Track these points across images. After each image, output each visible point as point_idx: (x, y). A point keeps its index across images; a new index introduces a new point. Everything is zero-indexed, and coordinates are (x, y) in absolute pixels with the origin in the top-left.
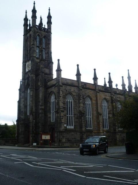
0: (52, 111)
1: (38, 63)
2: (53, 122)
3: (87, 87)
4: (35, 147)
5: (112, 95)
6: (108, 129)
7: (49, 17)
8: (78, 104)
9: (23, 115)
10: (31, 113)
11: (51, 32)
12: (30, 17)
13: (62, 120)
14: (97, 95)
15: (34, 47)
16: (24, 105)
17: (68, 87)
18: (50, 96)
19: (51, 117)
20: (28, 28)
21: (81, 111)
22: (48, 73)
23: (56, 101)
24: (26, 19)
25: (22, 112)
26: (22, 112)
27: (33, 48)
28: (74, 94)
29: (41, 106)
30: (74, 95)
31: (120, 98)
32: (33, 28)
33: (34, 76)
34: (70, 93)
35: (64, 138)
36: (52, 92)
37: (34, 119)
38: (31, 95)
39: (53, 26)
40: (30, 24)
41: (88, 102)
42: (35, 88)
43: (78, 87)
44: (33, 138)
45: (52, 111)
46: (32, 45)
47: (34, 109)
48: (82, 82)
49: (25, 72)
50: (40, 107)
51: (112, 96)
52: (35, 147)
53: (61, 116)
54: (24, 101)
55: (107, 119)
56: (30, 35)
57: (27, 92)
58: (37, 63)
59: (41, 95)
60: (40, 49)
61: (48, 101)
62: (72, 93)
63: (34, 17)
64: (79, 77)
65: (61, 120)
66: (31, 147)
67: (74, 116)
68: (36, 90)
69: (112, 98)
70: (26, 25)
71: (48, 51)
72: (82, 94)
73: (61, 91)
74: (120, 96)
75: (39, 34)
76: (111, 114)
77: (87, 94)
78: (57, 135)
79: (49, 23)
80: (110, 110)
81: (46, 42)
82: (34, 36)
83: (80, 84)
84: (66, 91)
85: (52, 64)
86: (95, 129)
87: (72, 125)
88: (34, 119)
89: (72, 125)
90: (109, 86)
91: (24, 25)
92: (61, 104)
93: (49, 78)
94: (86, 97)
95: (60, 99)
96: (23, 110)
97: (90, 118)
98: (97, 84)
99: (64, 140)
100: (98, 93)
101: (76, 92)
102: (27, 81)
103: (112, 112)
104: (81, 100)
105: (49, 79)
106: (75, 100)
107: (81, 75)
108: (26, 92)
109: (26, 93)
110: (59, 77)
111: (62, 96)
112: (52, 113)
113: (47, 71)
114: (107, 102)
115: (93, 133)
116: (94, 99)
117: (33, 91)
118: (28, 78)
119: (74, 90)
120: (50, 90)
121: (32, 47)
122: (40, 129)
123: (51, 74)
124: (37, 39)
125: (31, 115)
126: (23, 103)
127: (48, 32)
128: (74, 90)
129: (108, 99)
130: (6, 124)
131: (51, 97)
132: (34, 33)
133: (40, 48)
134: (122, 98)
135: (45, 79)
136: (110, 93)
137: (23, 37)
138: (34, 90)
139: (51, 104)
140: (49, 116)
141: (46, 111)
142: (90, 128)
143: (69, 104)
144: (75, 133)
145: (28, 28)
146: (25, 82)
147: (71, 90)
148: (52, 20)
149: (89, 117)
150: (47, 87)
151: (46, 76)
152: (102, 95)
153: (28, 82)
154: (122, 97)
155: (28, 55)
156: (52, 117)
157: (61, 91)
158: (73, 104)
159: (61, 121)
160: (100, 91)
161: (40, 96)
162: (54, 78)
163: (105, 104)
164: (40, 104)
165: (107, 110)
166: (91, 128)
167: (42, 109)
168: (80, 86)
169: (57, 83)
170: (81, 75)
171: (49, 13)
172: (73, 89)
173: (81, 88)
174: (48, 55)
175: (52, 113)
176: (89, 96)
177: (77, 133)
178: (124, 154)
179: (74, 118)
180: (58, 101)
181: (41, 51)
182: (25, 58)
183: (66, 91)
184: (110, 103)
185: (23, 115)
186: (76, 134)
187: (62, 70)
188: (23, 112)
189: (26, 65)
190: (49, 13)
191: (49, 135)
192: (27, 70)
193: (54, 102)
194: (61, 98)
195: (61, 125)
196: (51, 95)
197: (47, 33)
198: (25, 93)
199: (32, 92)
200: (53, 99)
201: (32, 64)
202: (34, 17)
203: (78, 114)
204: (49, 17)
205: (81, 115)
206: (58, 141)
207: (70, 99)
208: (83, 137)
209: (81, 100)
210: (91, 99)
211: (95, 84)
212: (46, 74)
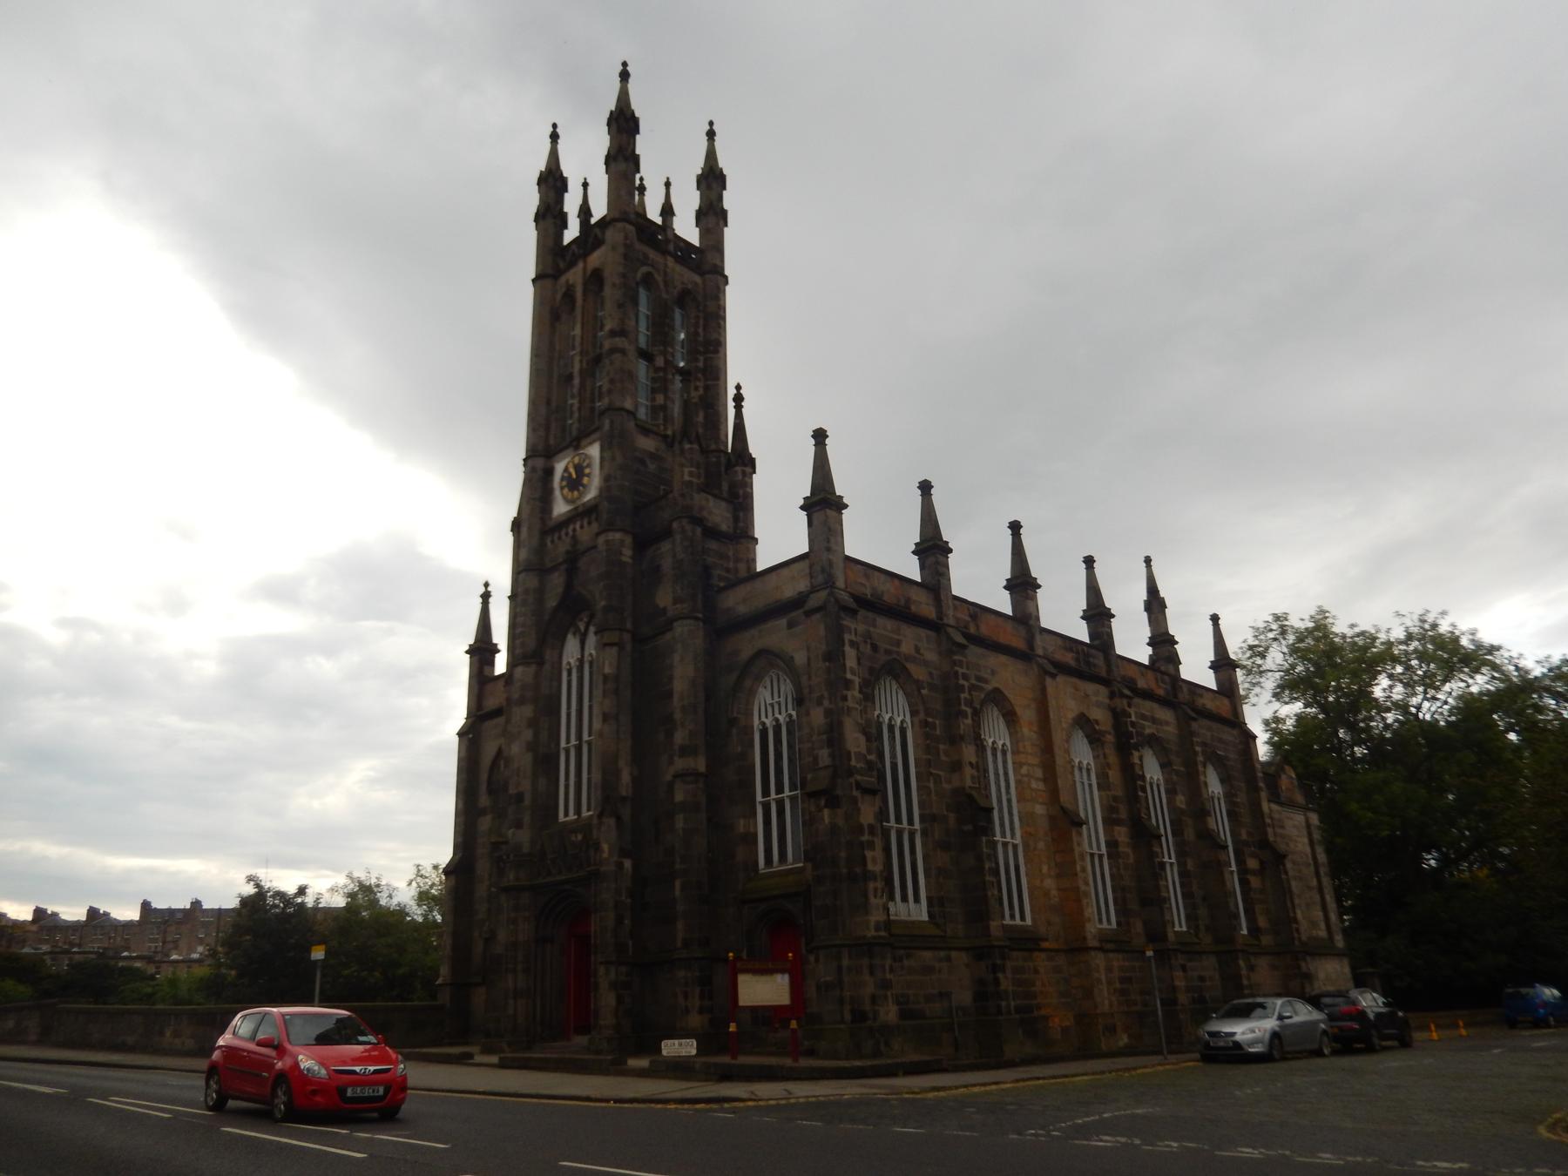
0: (766, 793)
1: (648, 461)
2: (779, 874)
3: (984, 630)
4: (680, 1069)
5: (1122, 696)
6: (1114, 925)
7: (712, 179)
8: (942, 747)
9: (527, 819)
10: (608, 801)
11: (723, 268)
12: (586, 165)
13: (869, 854)
14: (1043, 690)
15: (623, 352)
16: (532, 747)
17: (885, 626)
18: (748, 683)
19: (756, 835)
20: (572, 232)
21: (970, 797)
22: (724, 527)
23: (818, 717)
24: (552, 181)
25: (519, 797)
26: (519, 797)
27: (617, 356)
28: (918, 672)
29: (685, 751)
30: (919, 684)
31: (1154, 720)
32: (620, 225)
33: (628, 540)
34: (895, 669)
35: (886, 997)
36: (769, 658)
37: (624, 853)
38: (607, 670)
39: (732, 237)
40: (585, 211)
41: (996, 733)
42: (629, 626)
43: (936, 626)
44: (620, 1000)
45: (766, 793)
46: (613, 333)
47: (626, 777)
48: (956, 598)
49: (543, 520)
50: (680, 764)
51: (1121, 703)
52: (680, 1069)
53: (861, 827)
54: (533, 723)
55: (1101, 856)
56: (596, 279)
57: (560, 657)
58: (642, 462)
59: (683, 673)
60: (657, 370)
61: (733, 722)
62: (908, 665)
63: (622, 158)
64: (937, 563)
65: (864, 858)
66: (641, 1074)
67: (924, 833)
68: (642, 645)
69: (1118, 716)
70: (550, 215)
71: (706, 388)
72: (965, 677)
73: (847, 648)
74: (1155, 706)
75: (649, 274)
76: (1118, 822)
77: (986, 681)
78: (840, 969)
79: (712, 214)
80: (1115, 799)
81: (696, 334)
82: (624, 276)
83: (951, 612)
84: (875, 648)
85: (748, 470)
86: (1049, 923)
87: (917, 900)
88: (624, 853)
89: (917, 900)
90: (1091, 636)
91: (539, 217)
92: (854, 741)
93: (731, 565)
94: (983, 703)
95: (845, 698)
96: (526, 786)
97: (1015, 846)
98: (1038, 619)
99: (889, 1013)
100: (1049, 680)
101: (926, 663)
102: (557, 581)
103: (1123, 815)
104: (965, 715)
105: (728, 570)
106: (928, 714)
107: (951, 551)
108: (549, 655)
109: (547, 667)
110: (829, 549)
111: (857, 680)
112: (767, 807)
113: (718, 513)
114: (1095, 739)
115: (1043, 955)
116: (1027, 715)
117: (620, 645)
118: (572, 562)
119: (917, 650)
120: (746, 644)
121: (613, 350)
122: (680, 925)
123: (742, 535)
124: (626, 320)
125: (612, 822)
126: (528, 735)
127: (703, 269)
128: (917, 650)
129: (1097, 722)
130: (364, 894)
131: (752, 693)
132: (625, 256)
133: (660, 362)
134: (1167, 723)
135: (707, 570)
136: (1105, 682)
137: (528, 293)
138: (627, 637)
139: (752, 740)
140: (741, 825)
141: (725, 787)
142: (1018, 921)
143: (892, 738)
144: (942, 954)
145: (572, 232)
146: (540, 592)
147: (898, 643)
148: (729, 200)
149: (1011, 830)
150: (720, 628)
151: (713, 545)
152: (1067, 699)
153: (569, 586)
154: (1165, 714)
155: (560, 415)
156: (775, 840)
157: (853, 644)
158: (916, 746)
159: (865, 863)
160: (1063, 669)
161: (679, 686)
162: (760, 568)
163: (1082, 753)
164: (680, 737)
165: (1015, 812)
166: (1023, 918)
167: (696, 774)
168: (952, 622)
169: (814, 590)
170: (951, 551)
171: (711, 155)
172: (910, 640)
173: (960, 639)
174: (706, 417)
175: (767, 807)
176: (997, 698)
177: (954, 954)
178: (361, 1039)
179: (924, 844)
180: (828, 713)
181: (660, 385)
182: (547, 429)
183: (875, 648)
184: (1111, 752)
185: (527, 819)
186: (949, 959)
187: (845, 501)
188: (527, 802)
189: (549, 472)
190: (711, 155)
191: (782, 971)
192: (560, 508)
193: (777, 728)
194: (849, 694)
195: (866, 896)
196: (759, 678)
197: (697, 279)
198: (541, 663)
199: (614, 650)
200: (769, 705)
201: (613, 459)
202: (622, 158)
203: (952, 817)
204: (712, 179)
205: (964, 821)
206: (848, 1017)
207: (894, 708)
208: (997, 982)
209: (965, 715)
210: (1010, 717)
211: (1025, 616)
212: (711, 533)
